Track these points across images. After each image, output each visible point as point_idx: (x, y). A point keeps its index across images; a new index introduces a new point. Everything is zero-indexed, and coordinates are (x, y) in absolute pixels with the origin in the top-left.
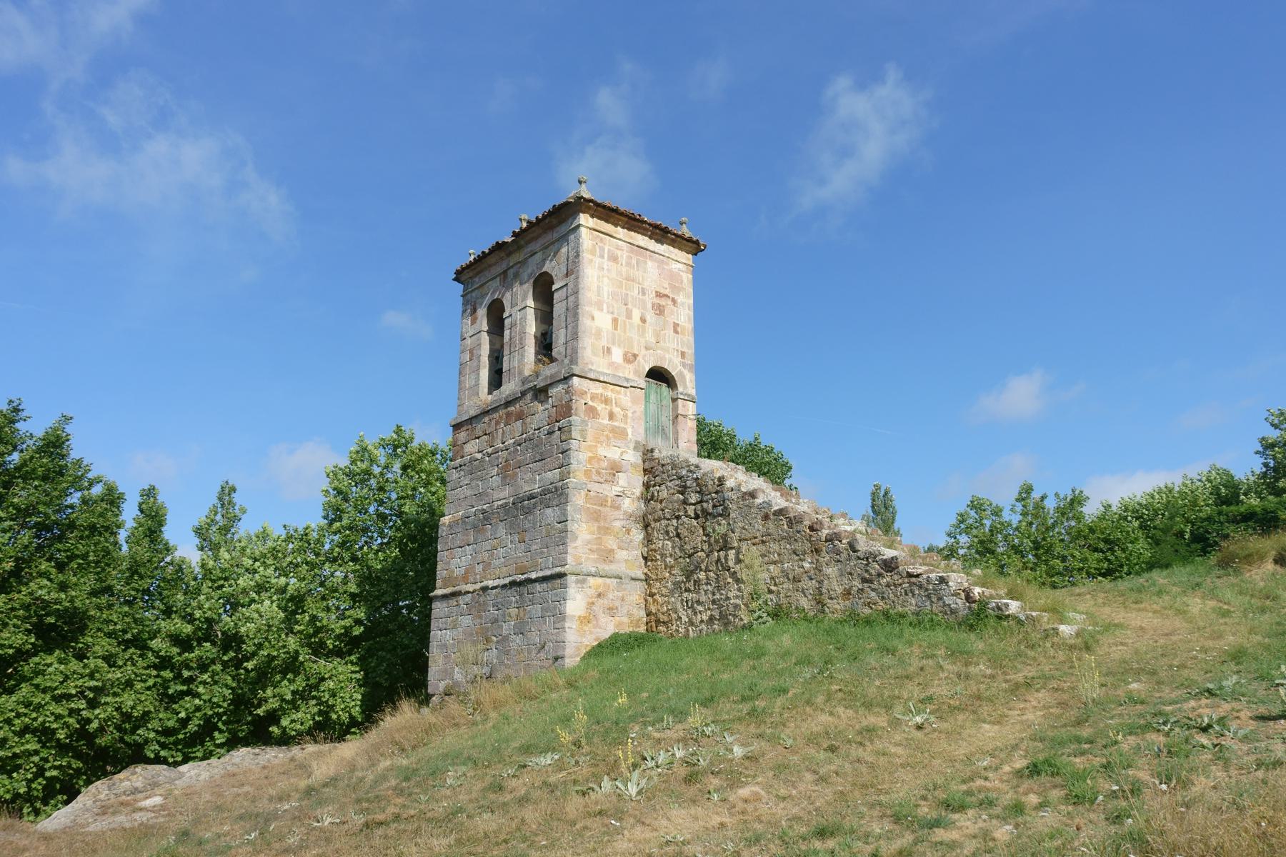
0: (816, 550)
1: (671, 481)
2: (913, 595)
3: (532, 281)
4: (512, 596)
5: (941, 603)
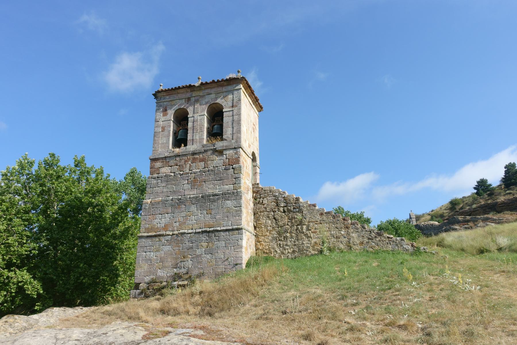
0: (347, 228)
1: (269, 197)
2: (390, 244)
3: (208, 105)
4: (204, 237)
5: (402, 247)
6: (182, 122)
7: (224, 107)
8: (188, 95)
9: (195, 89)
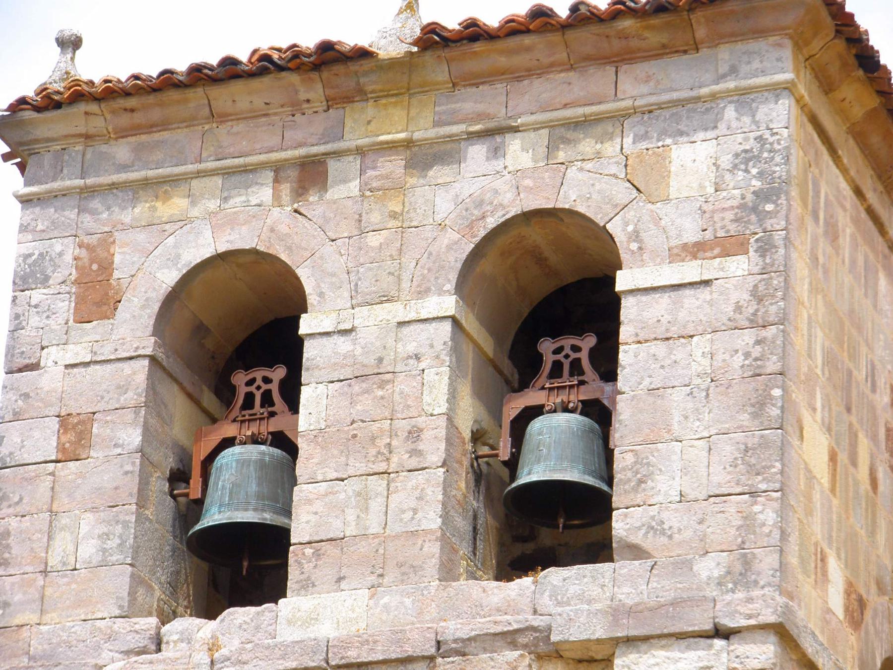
6: (239, 379)
9: (371, 83)
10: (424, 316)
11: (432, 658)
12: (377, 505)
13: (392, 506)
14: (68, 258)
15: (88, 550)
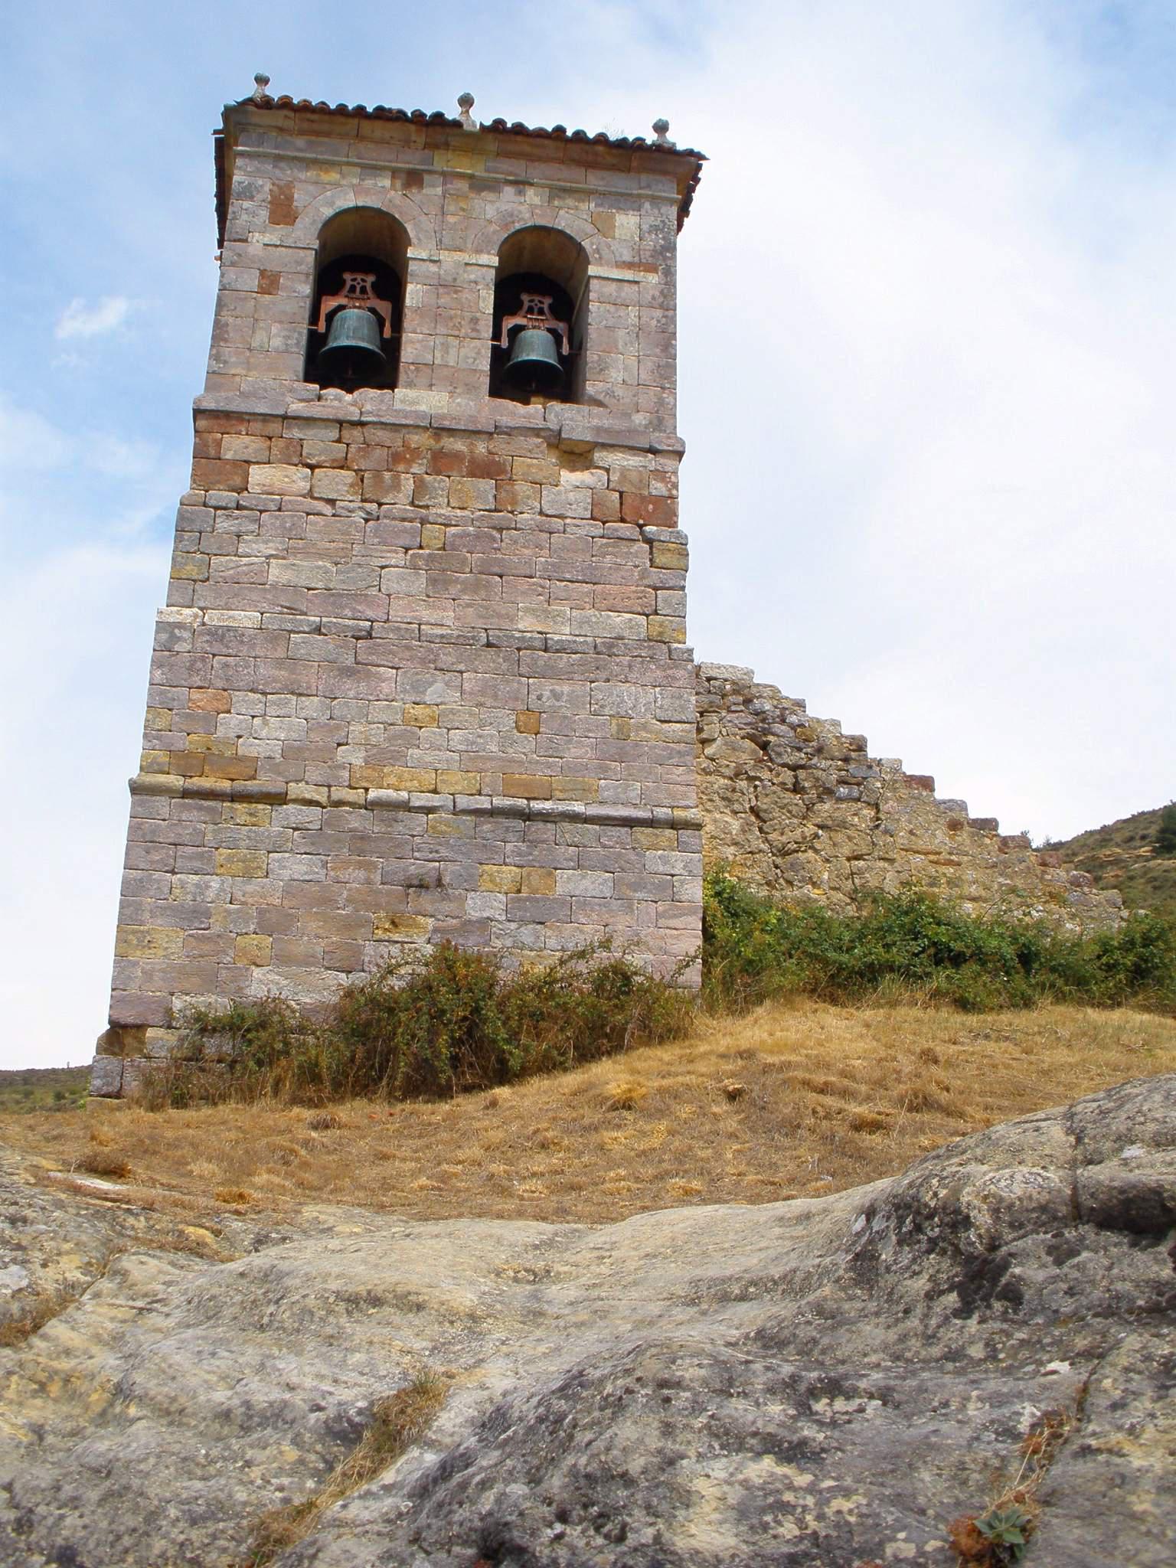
7: (593, 256)
8: (411, 160)
9: (454, 142)
10: (480, 263)
11: (491, 434)
12: (453, 351)
13: (461, 354)
14: (267, 188)
15: (277, 342)
